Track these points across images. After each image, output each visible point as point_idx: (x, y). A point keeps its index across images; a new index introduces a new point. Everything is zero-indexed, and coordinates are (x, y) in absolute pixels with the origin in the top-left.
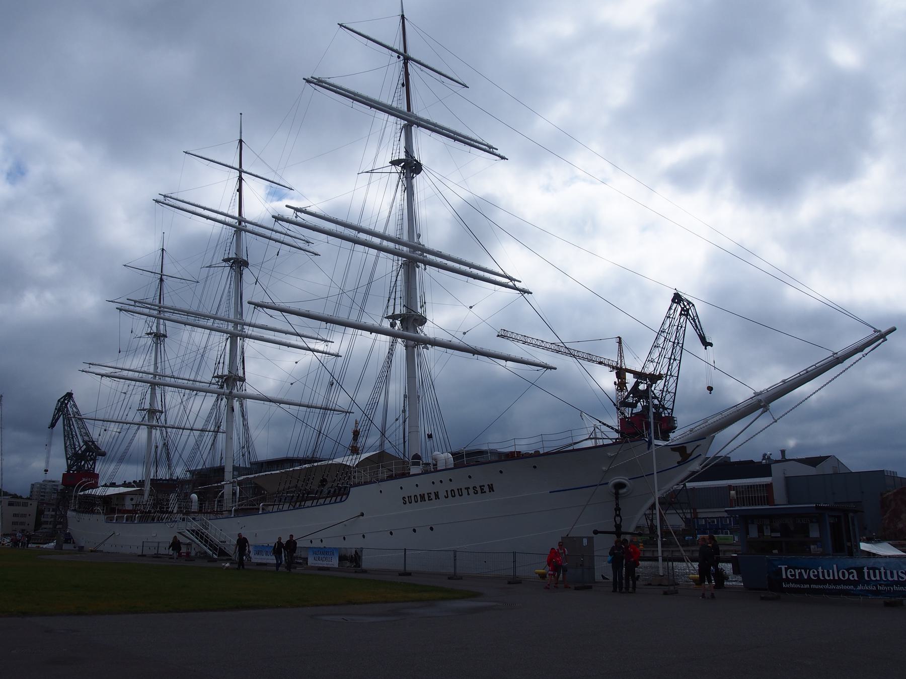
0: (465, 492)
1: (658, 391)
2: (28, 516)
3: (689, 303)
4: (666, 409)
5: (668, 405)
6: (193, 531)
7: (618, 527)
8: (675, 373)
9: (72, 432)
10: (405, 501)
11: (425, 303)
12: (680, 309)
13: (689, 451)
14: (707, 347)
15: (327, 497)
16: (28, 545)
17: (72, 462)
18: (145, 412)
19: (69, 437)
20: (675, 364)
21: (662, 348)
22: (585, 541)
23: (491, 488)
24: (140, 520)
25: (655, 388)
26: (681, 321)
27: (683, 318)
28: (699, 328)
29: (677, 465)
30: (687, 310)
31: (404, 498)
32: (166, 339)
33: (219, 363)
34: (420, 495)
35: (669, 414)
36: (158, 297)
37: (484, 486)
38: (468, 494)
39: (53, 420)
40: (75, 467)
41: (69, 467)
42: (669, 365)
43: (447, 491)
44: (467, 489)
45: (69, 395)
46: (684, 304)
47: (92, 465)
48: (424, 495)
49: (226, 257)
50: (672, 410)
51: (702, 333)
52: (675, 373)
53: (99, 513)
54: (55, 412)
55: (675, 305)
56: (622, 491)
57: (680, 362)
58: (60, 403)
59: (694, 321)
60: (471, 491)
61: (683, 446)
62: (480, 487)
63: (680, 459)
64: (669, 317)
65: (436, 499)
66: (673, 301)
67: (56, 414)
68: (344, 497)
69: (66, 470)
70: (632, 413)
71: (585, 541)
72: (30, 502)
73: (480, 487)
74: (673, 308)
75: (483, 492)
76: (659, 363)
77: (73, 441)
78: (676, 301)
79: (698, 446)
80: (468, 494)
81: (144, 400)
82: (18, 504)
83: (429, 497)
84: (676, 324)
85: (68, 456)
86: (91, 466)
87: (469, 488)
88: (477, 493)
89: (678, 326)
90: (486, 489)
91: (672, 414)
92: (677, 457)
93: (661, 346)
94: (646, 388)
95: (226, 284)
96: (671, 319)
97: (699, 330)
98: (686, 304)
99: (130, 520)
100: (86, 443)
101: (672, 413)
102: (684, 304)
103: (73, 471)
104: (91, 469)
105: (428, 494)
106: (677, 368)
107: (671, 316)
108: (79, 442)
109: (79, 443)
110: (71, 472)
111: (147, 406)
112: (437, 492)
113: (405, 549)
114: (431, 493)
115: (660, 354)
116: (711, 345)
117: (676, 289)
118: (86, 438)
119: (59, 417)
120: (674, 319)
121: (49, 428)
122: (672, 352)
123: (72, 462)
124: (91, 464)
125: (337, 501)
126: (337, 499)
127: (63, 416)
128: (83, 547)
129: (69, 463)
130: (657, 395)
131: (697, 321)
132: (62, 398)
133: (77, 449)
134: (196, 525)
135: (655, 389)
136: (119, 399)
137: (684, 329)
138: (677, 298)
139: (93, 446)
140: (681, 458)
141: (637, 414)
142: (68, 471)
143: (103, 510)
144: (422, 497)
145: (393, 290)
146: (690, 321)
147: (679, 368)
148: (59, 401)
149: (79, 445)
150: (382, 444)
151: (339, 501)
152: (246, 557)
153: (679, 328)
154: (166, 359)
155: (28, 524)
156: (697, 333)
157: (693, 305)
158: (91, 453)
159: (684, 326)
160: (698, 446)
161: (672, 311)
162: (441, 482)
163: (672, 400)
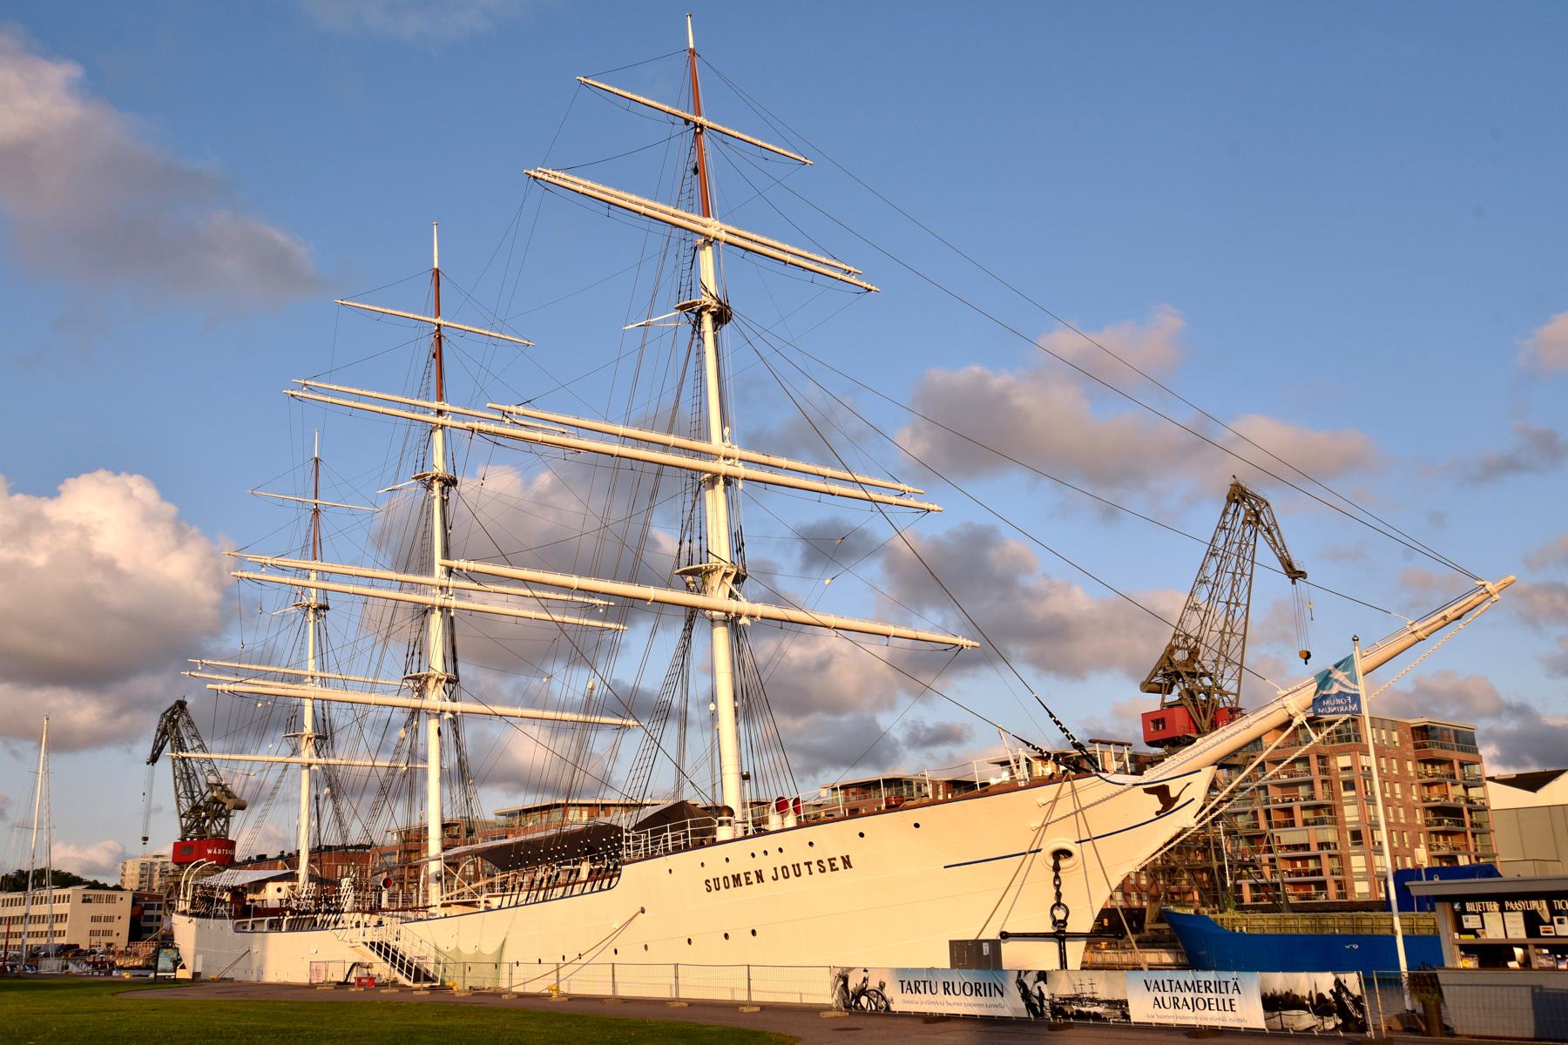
0: (804, 869)
1: (1209, 663)
2: (116, 918)
3: (1260, 500)
4: (1226, 694)
7: (1060, 924)
8: (1239, 629)
9: (187, 769)
11: (743, 544)
12: (1242, 513)
13: (1173, 794)
14: (1297, 580)
15: (568, 884)
17: (189, 822)
19: (182, 779)
20: (1240, 611)
22: (986, 948)
23: (847, 862)
24: (290, 926)
29: (1156, 817)
30: (1257, 515)
31: (707, 881)
32: (328, 612)
33: (413, 654)
34: (733, 876)
35: (1231, 702)
37: (835, 859)
38: (811, 873)
39: (153, 751)
40: (194, 831)
42: (1227, 616)
43: (775, 869)
44: (808, 864)
45: (181, 705)
46: (1250, 504)
48: (739, 875)
50: (1237, 695)
51: (1285, 554)
52: (1239, 629)
53: (223, 917)
55: (1234, 506)
56: (1063, 863)
58: (164, 720)
59: (1269, 532)
60: (814, 867)
61: (1164, 785)
62: (829, 860)
65: (845, 868)
66: (1231, 499)
68: (615, 879)
70: (1163, 704)
71: (986, 948)
72: (119, 894)
75: (833, 868)
77: (190, 784)
80: (811, 873)
82: (99, 899)
83: (747, 879)
84: (1237, 540)
85: (182, 812)
86: (222, 827)
88: (824, 871)
89: (1241, 543)
90: (839, 863)
91: (1237, 703)
92: (1155, 803)
94: (1187, 656)
96: (1227, 532)
97: (1280, 550)
98: (1253, 502)
99: (275, 926)
101: (1237, 700)
102: (1250, 504)
103: (192, 838)
104: (223, 834)
105: (745, 874)
106: (1243, 620)
108: (199, 787)
114: (749, 873)
116: (1302, 574)
117: (1234, 477)
119: (164, 744)
121: (148, 763)
123: (189, 822)
124: (222, 824)
125: (574, 893)
126: (574, 890)
130: (1209, 669)
131: (1275, 533)
132: (168, 711)
133: (197, 799)
134: (374, 935)
137: (1251, 548)
140: (1162, 806)
142: (183, 839)
144: (736, 879)
146: (1262, 534)
147: (1247, 618)
149: (201, 792)
150: (679, 787)
154: (330, 649)
155: (118, 934)
156: (1276, 553)
157: (1267, 504)
158: (221, 805)
160: (1188, 784)
161: (1229, 517)
162: (766, 853)
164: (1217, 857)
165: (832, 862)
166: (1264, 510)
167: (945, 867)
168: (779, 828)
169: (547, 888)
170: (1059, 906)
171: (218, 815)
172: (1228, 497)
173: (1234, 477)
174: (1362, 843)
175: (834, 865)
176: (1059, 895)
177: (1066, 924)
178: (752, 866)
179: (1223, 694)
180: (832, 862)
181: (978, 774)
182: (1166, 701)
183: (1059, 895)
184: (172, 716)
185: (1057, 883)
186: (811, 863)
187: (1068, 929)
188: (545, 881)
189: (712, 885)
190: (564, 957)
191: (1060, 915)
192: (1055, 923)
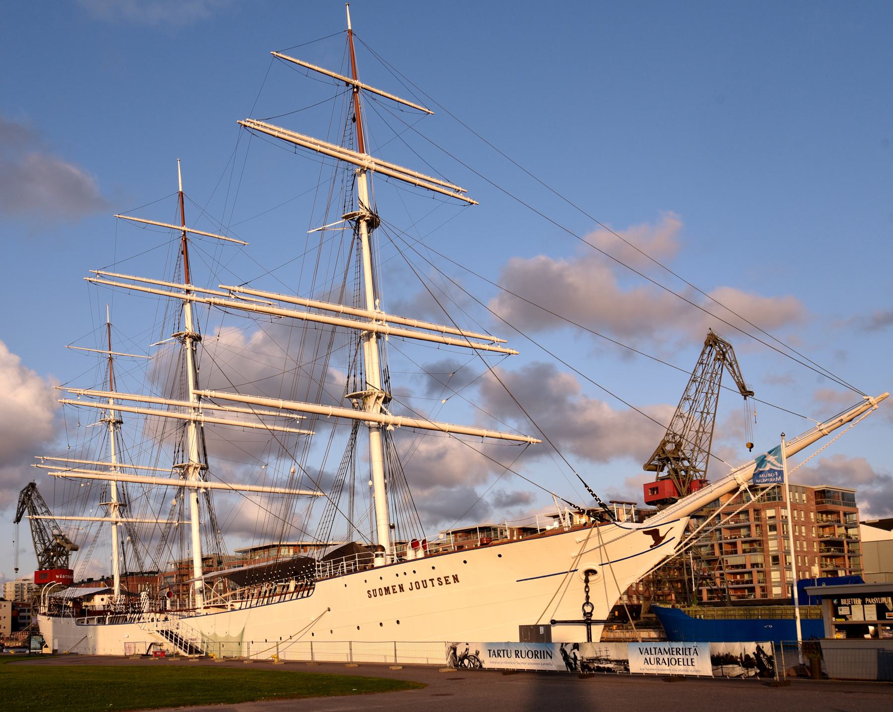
0: (429, 583)
4: (698, 471)
5: (700, 466)
6: (162, 631)
7: (588, 615)
8: (708, 429)
9: (39, 526)
10: (371, 595)
13: (661, 535)
16: (779, 602)
17: (43, 559)
21: (694, 400)
22: (542, 630)
23: (456, 579)
25: (685, 447)
26: (717, 367)
28: (738, 374)
32: (122, 425)
33: (178, 452)
34: (385, 588)
35: (701, 476)
37: (448, 577)
38: (433, 586)
39: (17, 515)
40: (47, 564)
41: (41, 564)
42: (701, 420)
43: (411, 583)
44: (432, 580)
45: (33, 485)
46: (720, 347)
47: (65, 560)
48: (388, 587)
50: (705, 472)
51: (741, 380)
53: (68, 616)
54: (18, 505)
55: (709, 348)
56: (591, 578)
57: (714, 416)
58: (23, 495)
60: (436, 582)
61: (656, 529)
62: (445, 578)
64: (702, 363)
65: (401, 591)
66: (707, 344)
67: (21, 507)
70: (657, 478)
71: (542, 630)
73: (445, 578)
74: (707, 352)
75: (447, 583)
76: (690, 419)
77: (42, 535)
80: (433, 586)
81: (105, 493)
83: (394, 590)
84: (710, 371)
87: (433, 579)
88: (442, 584)
90: (451, 580)
91: (705, 477)
92: (650, 540)
93: (692, 398)
94: (674, 447)
96: (704, 366)
97: (737, 377)
98: (722, 346)
99: (101, 621)
101: (705, 476)
102: (720, 347)
103: (46, 568)
105: (392, 587)
107: (705, 362)
108: (48, 537)
109: (49, 539)
110: (44, 569)
112: (402, 585)
113: (351, 642)
114: (395, 586)
115: (691, 407)
117: (710, 329)
120: (708, 365)
122: (705, 405)
123: (43, 559)
124: (64, 560)
125: (286, 600)
127: (28, 509)
128: (57, 650)
129: (40, 560)
131: (735, 366)
132: (24, 490)
133: (47, 544)
134: (162, 626)
135: (684, 449)
136: (78, 494)
140: (654, 542)
142: (40, 569)
143: (73, 612)
144: (387, 590)
145: (352, 366)
146: (726, 367)
147: (714, 422)
151: (288, 599)
152: (469, 661)
154: (125, 449)
155: (4, 627)
158: (62, 548)
160: (671, 528)
161: (705, 356)
162: (405, 574)
163: (704, 460)
165: (447, 578)
166: (729, 351)
167: (517, 581)
170: (588, 604)
173: (710, 329)
175: (448, 580)
176: (588, 597)
177: (591, 615)
178: (396, 582)
179: (696, 471)
180: (447, 578)
181: (358, 561)
183: (588, 597)
184: (27, 493)
185: (587, 590)
186: (433, 579)
187: (593, 618)
190: (281, 638)
191: (588, 609)
192: (585, 614)
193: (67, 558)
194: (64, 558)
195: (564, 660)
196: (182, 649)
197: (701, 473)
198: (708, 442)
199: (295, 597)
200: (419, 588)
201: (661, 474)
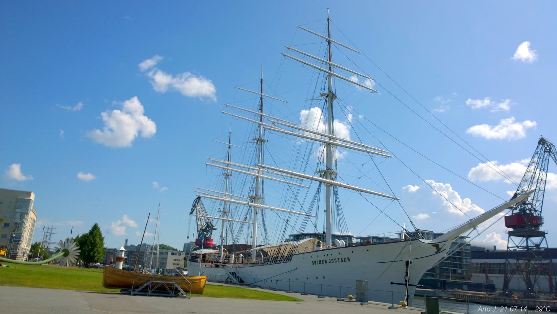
0: (337, 260)
12: (544, 148)
13: (440, 247)
18: (221, 213)
23: (349, 259)
27: (546, 154)
34: (319, 261)
35: (538, 214)
36: (228, 157)
38: (339, 262)
43: (330, 260)
44: (339, 259)
48: (321, 261)
49: (254, 138)
50: (541, 212)
60: (340, 260)
62: (344, 258)
63: (436, 250)
65: (348, 261)
66: (539, 143)
69: (197, 237)
70: (512, 213)
73: (344, 258)
78: (542, 143)
79: (444, 245)
80: (339, 262)
82: (176, 254)
89: (543, 159)
90: (347, 260)
91: (541, 215)
92: (435, 249)
95: (253, 154)
100: (207, 223)
110: (200, 238)
111: (222, 210)
117: (541, 135)
118: (207, 221)
132: (196, 199)
137: (547, 160)
138: (542, 141)
139: (210, 225)
141: (516, 214)
142: (198, 238)
144: (320, 262)
148: (194, 201)
153: (544, 160)
159: (548, 158)
160: (444, 245)
161: (539, 150)
162: (328, 255)
164: (454, 264)
166: (552, 148)
168: (312, 250)
169: (266, 262)
171: (209, 231)
172: (163, 245)
173: (541, 135)
174: (313, 264)
178: (324, 258)
179: (535, 211)
182: (514, 212)
184: (197, 201)
185: (407, 269)
188: (287, 257)
189: (314, 263)
193: (211, 234)
194: (210, 233)
195: (131, 245)
196: (235, 278)
197: (539, 212)
198: (542, 196)
199: (285, 261)
200: (333, 262)
201: (515, 211)
